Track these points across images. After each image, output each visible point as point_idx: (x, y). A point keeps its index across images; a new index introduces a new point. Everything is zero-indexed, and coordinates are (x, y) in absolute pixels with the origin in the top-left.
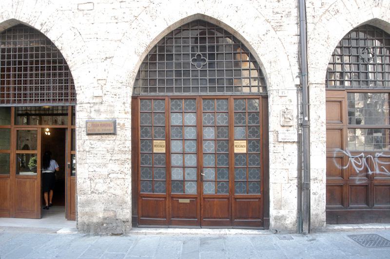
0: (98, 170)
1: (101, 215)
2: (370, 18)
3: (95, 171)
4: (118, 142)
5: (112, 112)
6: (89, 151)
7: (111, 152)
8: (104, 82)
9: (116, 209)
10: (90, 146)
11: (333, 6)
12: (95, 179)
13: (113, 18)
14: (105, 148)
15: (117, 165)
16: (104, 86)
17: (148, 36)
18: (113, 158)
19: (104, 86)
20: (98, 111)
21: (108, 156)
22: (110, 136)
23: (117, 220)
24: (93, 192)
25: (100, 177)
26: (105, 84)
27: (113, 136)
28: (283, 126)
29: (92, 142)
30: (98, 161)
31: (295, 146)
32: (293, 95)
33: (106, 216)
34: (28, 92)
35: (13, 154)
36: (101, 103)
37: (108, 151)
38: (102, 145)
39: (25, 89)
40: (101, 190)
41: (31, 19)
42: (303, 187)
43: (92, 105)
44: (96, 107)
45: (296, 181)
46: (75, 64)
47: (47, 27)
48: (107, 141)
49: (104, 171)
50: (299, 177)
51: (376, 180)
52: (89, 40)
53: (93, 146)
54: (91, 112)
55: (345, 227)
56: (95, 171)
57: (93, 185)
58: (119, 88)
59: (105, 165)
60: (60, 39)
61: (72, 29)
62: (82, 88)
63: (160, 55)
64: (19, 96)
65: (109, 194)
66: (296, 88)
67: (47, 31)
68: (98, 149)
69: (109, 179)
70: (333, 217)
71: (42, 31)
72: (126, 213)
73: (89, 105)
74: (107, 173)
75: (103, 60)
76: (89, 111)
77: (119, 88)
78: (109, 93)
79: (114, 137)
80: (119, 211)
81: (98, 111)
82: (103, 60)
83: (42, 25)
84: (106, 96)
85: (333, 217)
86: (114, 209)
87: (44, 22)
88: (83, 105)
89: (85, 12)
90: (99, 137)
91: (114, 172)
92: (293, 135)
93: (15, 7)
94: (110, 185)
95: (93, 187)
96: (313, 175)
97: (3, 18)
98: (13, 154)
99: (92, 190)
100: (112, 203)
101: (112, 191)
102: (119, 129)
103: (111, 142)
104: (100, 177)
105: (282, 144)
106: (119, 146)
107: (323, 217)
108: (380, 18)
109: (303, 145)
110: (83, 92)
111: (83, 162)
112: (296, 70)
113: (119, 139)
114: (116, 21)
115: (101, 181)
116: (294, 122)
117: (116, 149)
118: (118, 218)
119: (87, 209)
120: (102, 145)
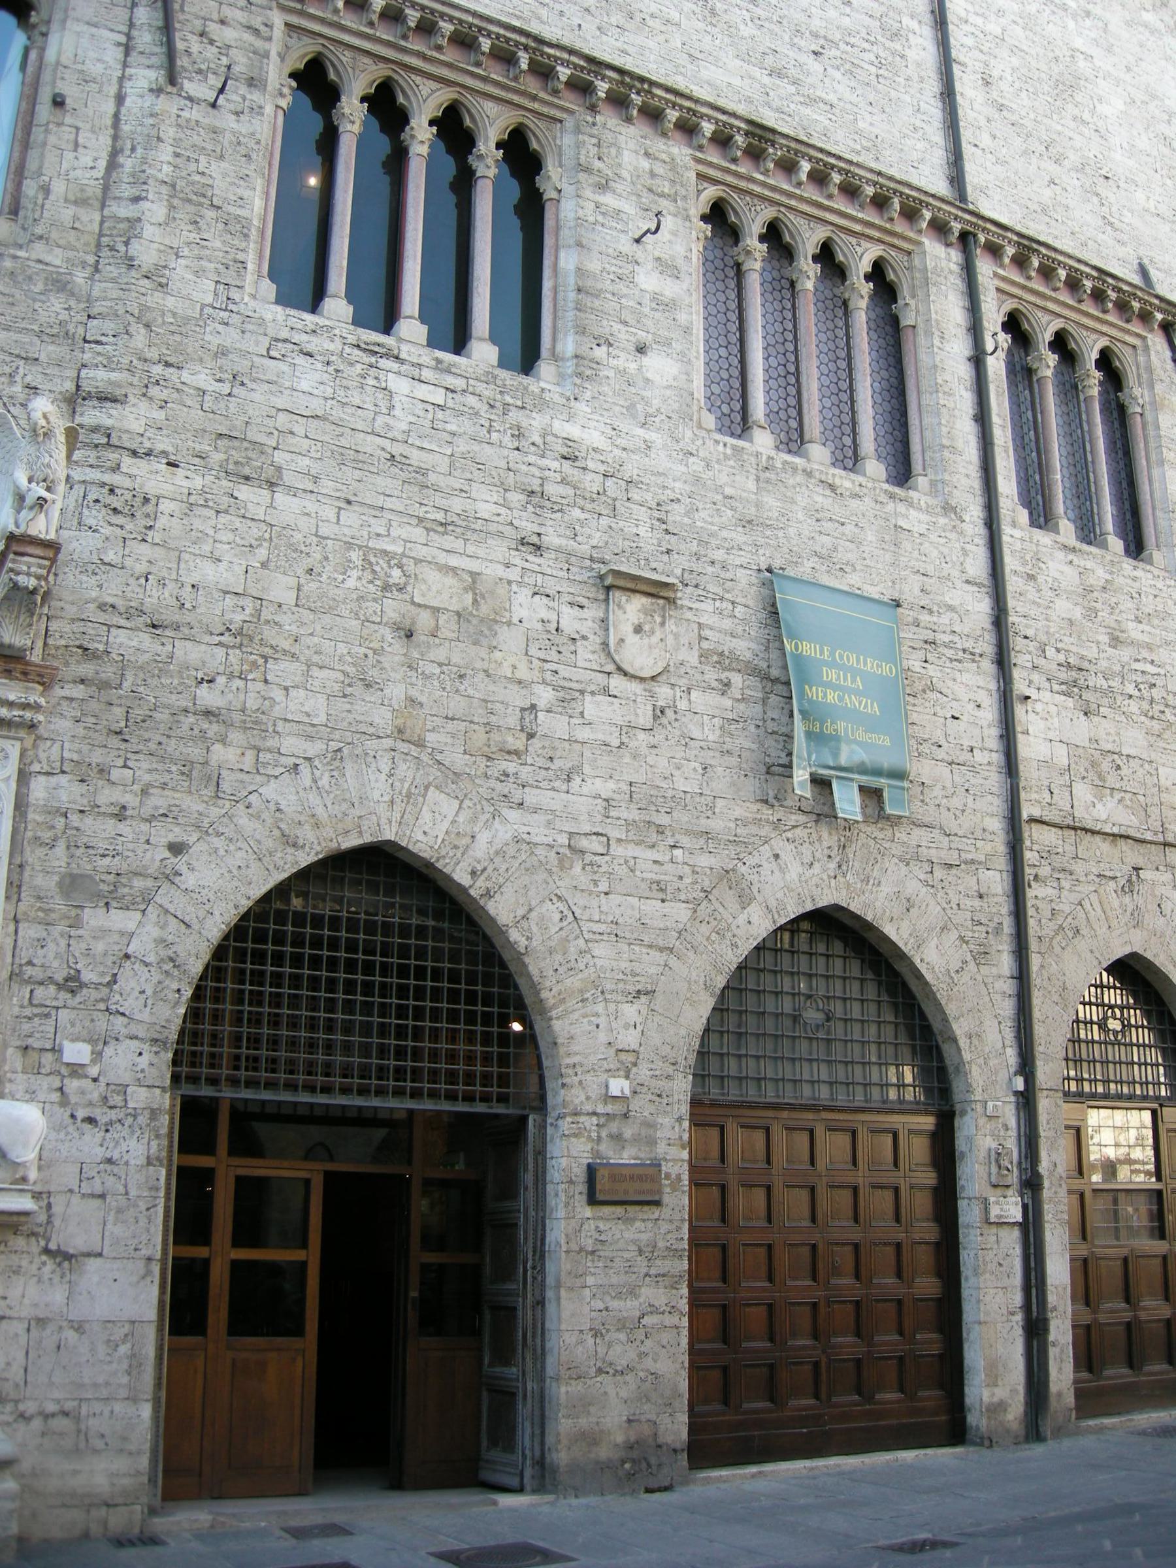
0: (615, 1304)
1: (620, 1438)
2: (1127, 950)
3: (607, 1309)
4: (665, 1227)
5: (652, 1142)
6: (593, 1252)
7: (647, 1251)
8: (631, 1058)
9: (658, 1415)
10: (597, 1236)
11: (1069, 919)
12: (608, 1331)
13: (654, 886)
14: (634, 1242)
15: (662, 1290)
16: (634, 1070)
17: (734, 946)
18: (653, 1271)
19: (634, 1070)
20: (617, 1138)
21: (641, 1265)
22: (646, 1208)
23: (659, 1446)
24: (600, 1371)
25: (622, 1325)
26: (635, 1064)
27: (654, 1208)
28: (995, 1186)
29: (602, 1226)
30: (615, 1280)
31: (1016, 1233)
32: (1009, 1114)
33: (632, 1439)
34: (282, 1054)
35: (219, 1260)
36: (626, 1116)
37: (641, 1252)
38: (626, 1235)
39: (274, 1042)
40: (622, 1363)
41: (443, 853)
42: (1035, 1329)
43: (602, 1120)
44: (614, 1127)
45: (1019, 1317)
46: (563, 1001)
47: (489, 884)
48: (638, 1224)
49: (629, 1307)
50: (1027, 1307)
51: (1145, 1309)
52: (597, 937)
53: (602, 1238)
54: (599, 1138)
55: (1107, 1421)
56: (607, 1309)
57: (601, 1350)
58: (668, 1077)
59: (633, 1292)
60: (524, 924)
61: (555, 899)
62: (579, 1069)
63: (745, 997)
64: (251, 1064)
65: (642, 1374)
66: (1013, 1099)
67: (488, 894)
68: (615, 1247)
69: (642, 1331)
70: (1090, 1400)
71: (472, 892)
72: (676, 1427)
73: (594, 1120)
74: (638, 1314)
75: (630, 998)
76: (594, 1135)
77: (668, 1077)
78: (645, 1090)
79: (655, 1212)
80: (665, 1421)
81: (617, 1138)
82: (630, 998)
83: (473, 873)
84: (637, 1097)
85: (1090, 1400)
86: (653, 1417)
87: (479, 868)
88: (582, 1119)
89: (588, 858)
90: (619, 1210)
91: (654, 1310)
92: (1012, 1208)
93: (398, 808)
94: (642, 1349)
95: (600, 1355)
96: (1051, 1299)
97: (360, 832)
98: (219, 1260)
99: (599, 1364)
100: (648, 1400)
101: (649, 1363)
102: (668, 1190)
103: (650, 1225)
104: (622, 1325)
105: (994, 1230)
106: (669, 1236)
107: (1070, 1399)
108: (1141, 952)
109: (1031, 1229)
110: (580, 1082)
111: (579, 1282)
112: (1011, 1056)
113: (667, 1217)
114: (661, 895)
115: (622, 1336)
116: (1014, 1178)
117: (661, 1244)
118: (660, 1440)
119: (583, 1422)
120: (626, 1235)
